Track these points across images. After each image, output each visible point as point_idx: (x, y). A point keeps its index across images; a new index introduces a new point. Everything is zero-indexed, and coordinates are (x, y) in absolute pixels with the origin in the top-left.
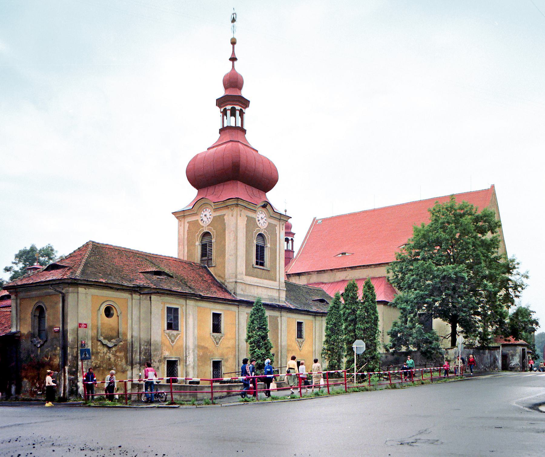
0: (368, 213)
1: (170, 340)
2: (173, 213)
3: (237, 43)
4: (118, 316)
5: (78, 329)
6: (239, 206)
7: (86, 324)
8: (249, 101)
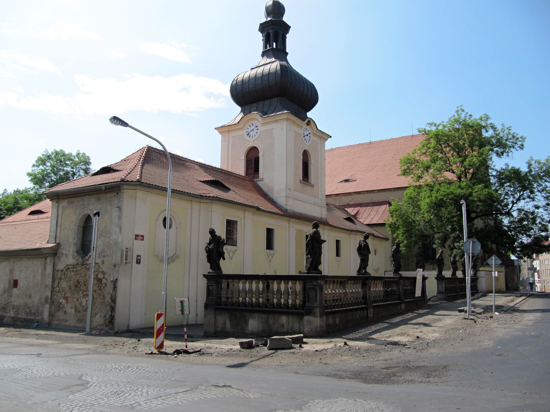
0: (364, 146)
4: (177, 228)
6: (290, 120)
7: (143, 236)
8: (290, 27)
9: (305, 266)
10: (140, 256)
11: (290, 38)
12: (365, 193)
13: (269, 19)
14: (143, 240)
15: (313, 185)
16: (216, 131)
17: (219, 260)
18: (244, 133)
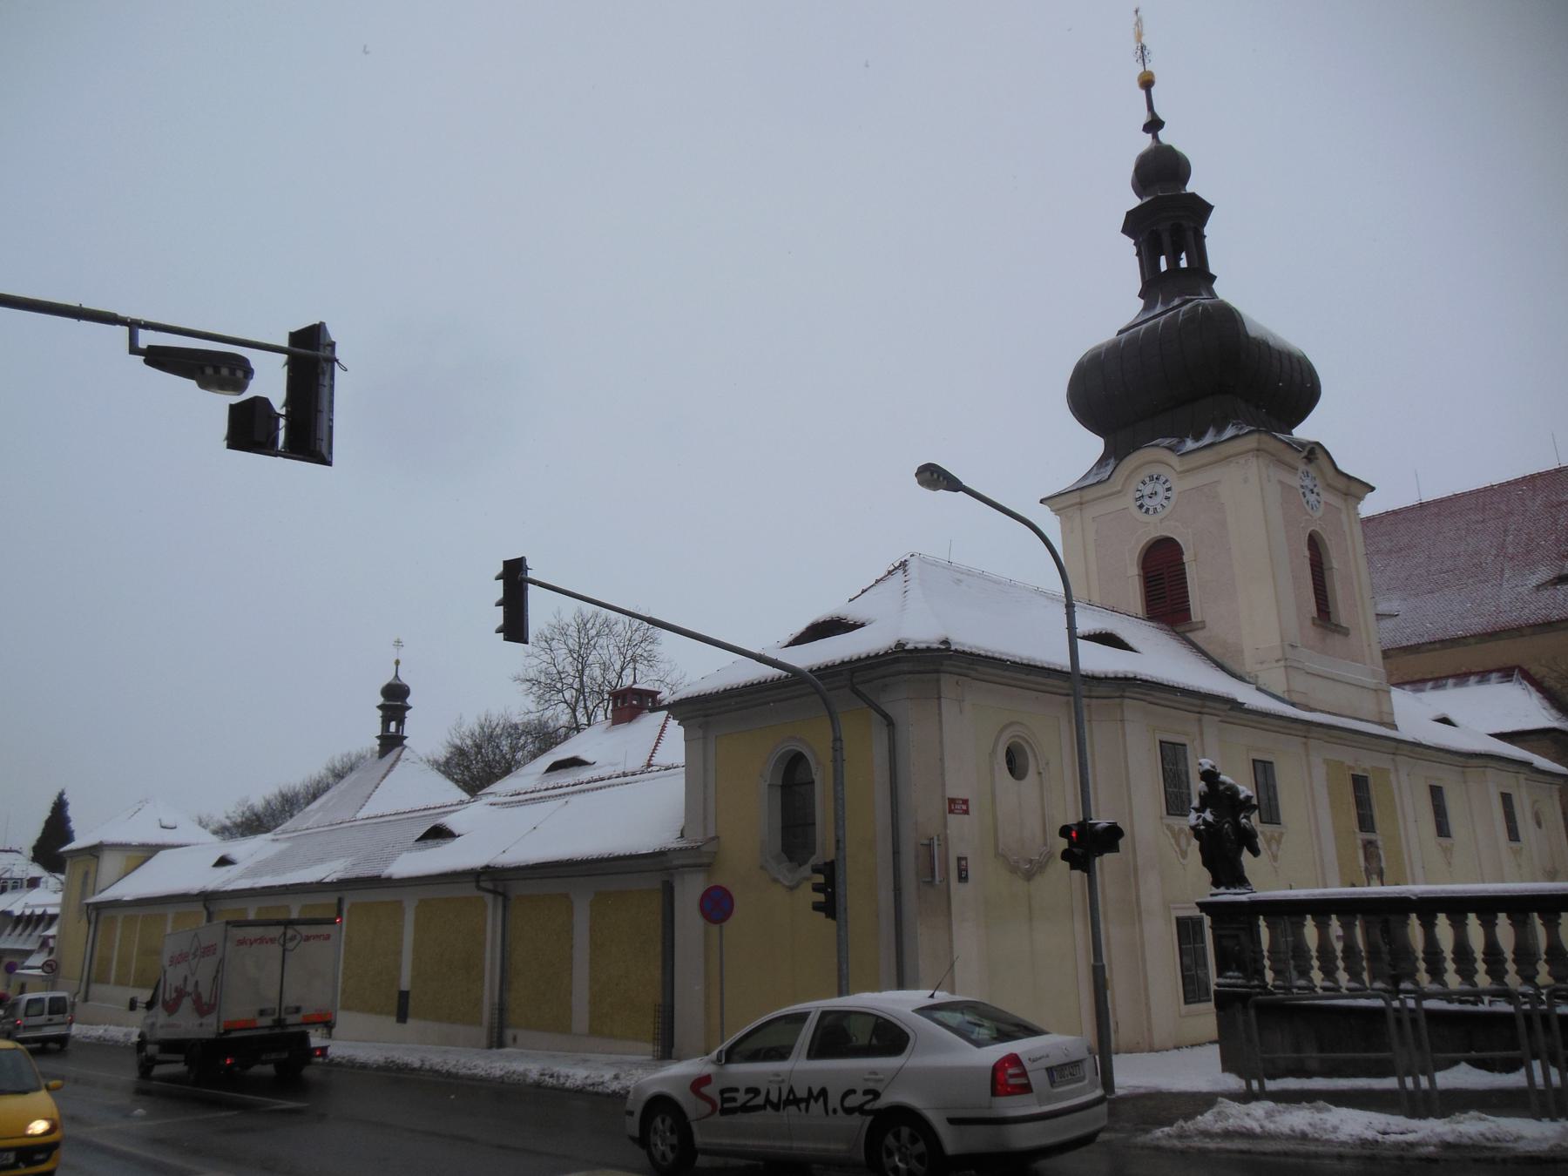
1: (1177, 850)
2: (61, 795)
3: (1156, 80)
4: (1040, 773)
5: (945, 818)
7: (965, 802)
9: (1363, 869)
10: (966, 859)
11: (1213, 231)
12: (1435, 650)
13: (1146, 199)
14: (966, 812)
15: (1347, 629)
16: (1045, 508)
17: (1240, 852)
18: (1128, 501)
